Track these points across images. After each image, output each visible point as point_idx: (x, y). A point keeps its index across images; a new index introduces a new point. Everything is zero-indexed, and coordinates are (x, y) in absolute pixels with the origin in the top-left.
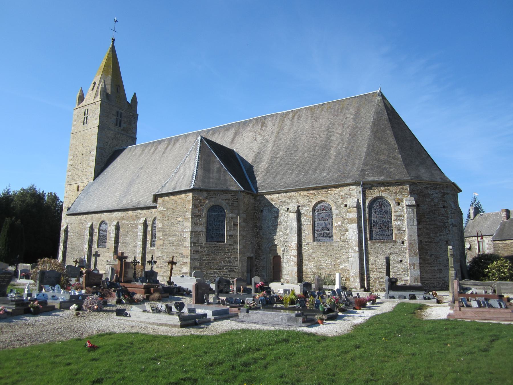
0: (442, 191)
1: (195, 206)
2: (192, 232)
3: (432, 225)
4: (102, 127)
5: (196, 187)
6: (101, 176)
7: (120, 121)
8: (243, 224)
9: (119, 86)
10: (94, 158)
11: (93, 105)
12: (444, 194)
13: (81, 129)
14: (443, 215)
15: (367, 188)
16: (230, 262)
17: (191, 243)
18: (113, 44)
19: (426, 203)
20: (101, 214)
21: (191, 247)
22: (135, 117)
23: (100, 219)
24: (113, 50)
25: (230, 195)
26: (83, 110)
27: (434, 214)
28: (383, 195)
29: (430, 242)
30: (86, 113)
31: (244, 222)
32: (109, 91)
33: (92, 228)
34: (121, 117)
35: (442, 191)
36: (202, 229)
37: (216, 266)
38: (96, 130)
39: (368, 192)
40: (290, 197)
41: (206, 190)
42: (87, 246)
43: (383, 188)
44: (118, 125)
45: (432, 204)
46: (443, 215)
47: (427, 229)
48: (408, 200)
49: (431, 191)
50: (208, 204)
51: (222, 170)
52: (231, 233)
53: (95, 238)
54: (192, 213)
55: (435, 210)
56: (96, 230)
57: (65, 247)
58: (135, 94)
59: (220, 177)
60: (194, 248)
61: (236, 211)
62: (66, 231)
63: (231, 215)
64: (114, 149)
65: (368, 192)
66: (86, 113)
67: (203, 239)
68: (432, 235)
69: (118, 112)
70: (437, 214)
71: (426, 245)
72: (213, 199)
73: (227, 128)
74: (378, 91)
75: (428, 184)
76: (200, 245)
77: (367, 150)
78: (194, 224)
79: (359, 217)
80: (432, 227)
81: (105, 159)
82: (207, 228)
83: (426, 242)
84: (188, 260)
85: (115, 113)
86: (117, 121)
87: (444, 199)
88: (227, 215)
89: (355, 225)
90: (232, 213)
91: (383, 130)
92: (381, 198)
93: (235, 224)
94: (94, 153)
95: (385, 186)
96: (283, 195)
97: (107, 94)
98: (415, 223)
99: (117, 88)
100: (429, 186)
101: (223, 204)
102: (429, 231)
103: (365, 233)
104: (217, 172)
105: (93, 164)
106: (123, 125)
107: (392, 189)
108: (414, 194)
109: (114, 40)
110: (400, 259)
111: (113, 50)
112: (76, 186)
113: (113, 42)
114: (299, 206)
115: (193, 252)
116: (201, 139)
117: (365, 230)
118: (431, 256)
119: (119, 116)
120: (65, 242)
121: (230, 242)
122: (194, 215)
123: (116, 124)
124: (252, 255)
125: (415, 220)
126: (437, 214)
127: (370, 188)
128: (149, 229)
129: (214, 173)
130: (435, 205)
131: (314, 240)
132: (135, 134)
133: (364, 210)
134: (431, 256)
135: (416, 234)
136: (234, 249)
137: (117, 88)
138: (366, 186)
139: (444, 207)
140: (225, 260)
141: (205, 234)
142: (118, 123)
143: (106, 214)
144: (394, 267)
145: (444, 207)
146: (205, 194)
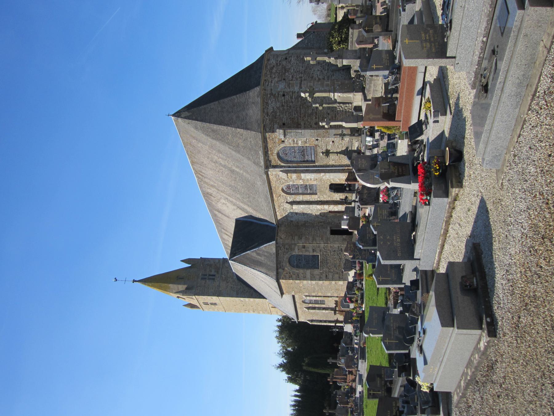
0: (269, 96)
1: (290, 278)
2: (311, 280)
3: (301, 111)
4: (219, 294)
5: (275, 277)
6: (265, 296)
7: (210, 275)
8: (303, 240)
9: (178, 277)
10: (247, 299)
11: (199, 300)
12: (271, 94)
13: (221, 307)
14: (292, 98)
15: (270, 164)
16: (335, 251)
17: (320, 280)
18: (138, 281)
19: (281, 116)
20: (297, 303)
21: (323, 280)
22: (203, 260)
23: (300, 304)
24: (145, 281)
25: (280, 251)
26: (203, 306)
27: (290, 107)
28: (276, 152)
29: (316, 113)
30: (206, 304)
31: (301, 239)
32: (182, 287)
33: (308, 308)
34: (206, 275)
35: (269, 96)
36: (308, 272)
37: (338, 262)
38: (221, 298)
39: (273, 163)
40: (279, 206)
41: (277, 269)
42: (324, 311)
43: (269, 152)
44: (213, 277)
45: (281, 109)
46: (292, 98)
47: (305, 116)
48: (279, 134)
49: (270, 110)
50: (288, 268)
51: (258, 252)
52: (311, 250)
53: (317, 306)
54: (296, 280)
55: (287, 106)
56: (310, 305)
57: (325, 321)
58: (182, 261)
59: (265, 256)
60: (324, 278)
61: (293, 246)
62: (312, 321)
63: (296, 250)
64: (236, 281)
65: (273, 163)
66: (206, 304)
67: (316, 272)
68: (310, 112)
69: (202, 279)
70: (291, 104)
71: (319, 118)
72: (284, 264)
73: (217, 221)
74: (173, 118)
75: (264, 112)
76: (321, 274)
77: (235, 151)
78: (305, 278)
79: (295, 172)
80: (302, 111)
81: (247, 289)
82: (308, 268)
83: (316, 118)
84: (333, 282)
85: (204, 282)
86: (210, 279)
87: (277, 95)
88: (296, 252)
89: (303, 175)
90: (294, 249)
91: (213, 131)
92: (278, 154)
93: (304, 247)
94: (242, 299)
95: (268, 151)
96: (277, 210)
97: (187, 289)
98: (300, 131)
99: (180, 278)
100: (266, 111)
101: (287, 256)
102: (306, 115)
103: (309, 167)
104: (261, 256)
105: (252, 300)
106: (213, 273)
107: (270, 145)
108: (273, 128)
109: (134, 281)
110: (331, 143)
111: (145, 281)
112: (272, 309)
113: (136, 281)
114: (287, 202)
115: (327, 278)
116: (232, 260)
117: (306, 167)
118: (328, 114)
119: (206, 277)
120: (321, 321)
121: (319, 251)
122: (298, 278)
123: (214, 279)
124: (329, 228)
125: (297, 131)
126: (291, 104)
127: (270, 161)
128: (310, 305)
129: (261, 259)
130: (283, 106)
131: (316, 194)
132: (219, 260)
133: (289, 167)
134: (328, 114)
135: (309, 131)
136: (324, 248)
137: (180, 278)
138: (268, 165)
139: (284, 95)
140: (334, 255)
141: (312, 270)
142: (212, 277)
143: (296, 300)
144: (338, 147)
145: (284, 95)
146: (280, 270)
